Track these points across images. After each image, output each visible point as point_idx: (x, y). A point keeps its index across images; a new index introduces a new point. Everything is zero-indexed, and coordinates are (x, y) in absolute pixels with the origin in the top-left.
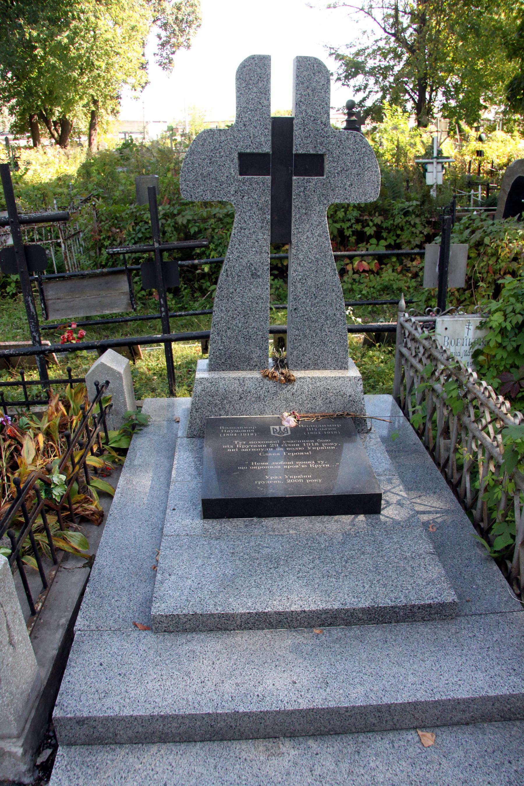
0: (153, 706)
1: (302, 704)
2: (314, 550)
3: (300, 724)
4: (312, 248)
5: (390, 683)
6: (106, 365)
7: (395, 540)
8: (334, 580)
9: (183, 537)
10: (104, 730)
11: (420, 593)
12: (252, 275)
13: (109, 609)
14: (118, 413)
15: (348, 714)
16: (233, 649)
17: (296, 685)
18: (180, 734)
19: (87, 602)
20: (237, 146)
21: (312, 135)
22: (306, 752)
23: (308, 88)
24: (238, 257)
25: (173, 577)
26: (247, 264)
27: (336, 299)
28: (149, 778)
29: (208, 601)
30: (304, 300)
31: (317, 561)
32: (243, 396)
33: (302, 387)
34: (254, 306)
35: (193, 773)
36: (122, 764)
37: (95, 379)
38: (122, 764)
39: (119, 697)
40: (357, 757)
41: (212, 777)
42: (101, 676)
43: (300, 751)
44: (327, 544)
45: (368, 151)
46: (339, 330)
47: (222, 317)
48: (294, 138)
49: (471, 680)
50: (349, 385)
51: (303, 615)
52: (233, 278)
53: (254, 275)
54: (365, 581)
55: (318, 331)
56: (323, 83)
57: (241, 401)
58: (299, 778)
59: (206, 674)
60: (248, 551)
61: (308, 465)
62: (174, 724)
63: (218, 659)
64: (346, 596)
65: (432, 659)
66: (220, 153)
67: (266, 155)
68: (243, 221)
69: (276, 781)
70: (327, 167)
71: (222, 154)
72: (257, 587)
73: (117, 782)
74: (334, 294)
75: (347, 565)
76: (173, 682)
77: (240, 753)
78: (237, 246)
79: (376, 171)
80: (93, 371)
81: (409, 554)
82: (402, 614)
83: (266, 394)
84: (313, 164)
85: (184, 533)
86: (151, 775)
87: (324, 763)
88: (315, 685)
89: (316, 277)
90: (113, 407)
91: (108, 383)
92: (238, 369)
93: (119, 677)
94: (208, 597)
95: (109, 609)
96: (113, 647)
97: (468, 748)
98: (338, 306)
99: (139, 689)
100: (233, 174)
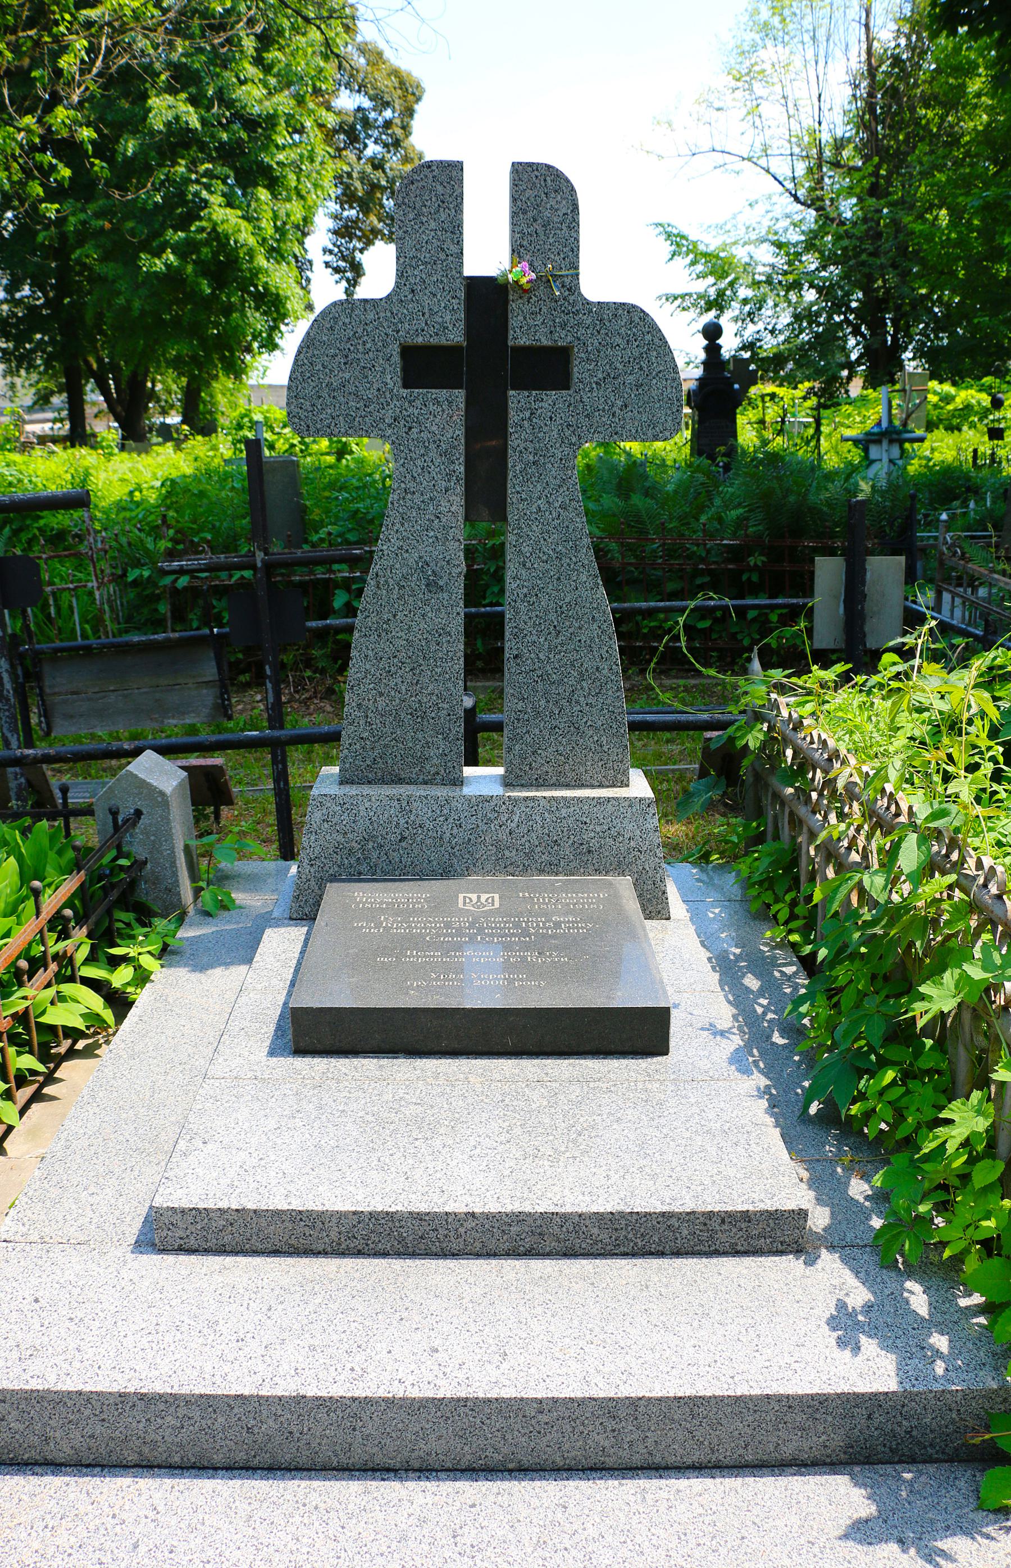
0: (127, 1377)
1: (442, 1390)
2: (514, 1111)
3: (440, 1438)
4: (548, 532)
5: (641, 1361)
6: (136, 776)
7: (693, 1100)
8: (546, 1163)
10: (22, 1427)
11: (728, 1191)
12: (427, 585)
13: (74, 1207)
14: (157, 878)
15: (544, 1418)
16: (317, 1287)
17: (436, 1355)
18: (181, 1445)
20: (398, 332)
21: (544, 309)
22: (450, 1501)
23: (535, 220)
24: (401, 548)
25: (209, 1146)
28: (102, 1531)
30: (535, 638)
31: (518, 1131)
33: (529, 817)
34: (433, 649)
36: (54, 1501)
38: (54, 1501)
39: (62, 1357)
40: (560, 1515)
41: (239, 1536)
42: (32, 1321)
43: (437, 1498)
44: (545, 1103)
46: (609, 701)
49: (822, 1362)
50: (629, 815)
51: (470, 1224)
54: (614, 1166)
55: (564, 702)
56: (564, 211)
57: (403, 844)
58: (427, 1548)
59: (250, 1327)
62: (169, 1418)
63: (281, 1303)
64: (567, 1192)
65: (742, 1321)
68: (408, 476)
69: (374, 1551)
70: (578, 370)
71: (368, 346)
72: (384, 1169)
73: (34, 1534)
74: (595, 626)
75: (580, 1139)
77: (306, 1495)
78: (398, 526)
81: (718, 1125)
83: (455, 831)
84: (550, 368)
85: (250, 1075)
86: (109, 1526)
87: (485, 1523)
89: (558, 591)
90: (149, 866)
91: (138, 813)
92: (400, 781)
93: (68, 1324)
94: (274, 1182)
95: (74, 1207)
96: (67, 1273)
97: (811, 1510)
98: (603, 652)
99: (106, 1345)
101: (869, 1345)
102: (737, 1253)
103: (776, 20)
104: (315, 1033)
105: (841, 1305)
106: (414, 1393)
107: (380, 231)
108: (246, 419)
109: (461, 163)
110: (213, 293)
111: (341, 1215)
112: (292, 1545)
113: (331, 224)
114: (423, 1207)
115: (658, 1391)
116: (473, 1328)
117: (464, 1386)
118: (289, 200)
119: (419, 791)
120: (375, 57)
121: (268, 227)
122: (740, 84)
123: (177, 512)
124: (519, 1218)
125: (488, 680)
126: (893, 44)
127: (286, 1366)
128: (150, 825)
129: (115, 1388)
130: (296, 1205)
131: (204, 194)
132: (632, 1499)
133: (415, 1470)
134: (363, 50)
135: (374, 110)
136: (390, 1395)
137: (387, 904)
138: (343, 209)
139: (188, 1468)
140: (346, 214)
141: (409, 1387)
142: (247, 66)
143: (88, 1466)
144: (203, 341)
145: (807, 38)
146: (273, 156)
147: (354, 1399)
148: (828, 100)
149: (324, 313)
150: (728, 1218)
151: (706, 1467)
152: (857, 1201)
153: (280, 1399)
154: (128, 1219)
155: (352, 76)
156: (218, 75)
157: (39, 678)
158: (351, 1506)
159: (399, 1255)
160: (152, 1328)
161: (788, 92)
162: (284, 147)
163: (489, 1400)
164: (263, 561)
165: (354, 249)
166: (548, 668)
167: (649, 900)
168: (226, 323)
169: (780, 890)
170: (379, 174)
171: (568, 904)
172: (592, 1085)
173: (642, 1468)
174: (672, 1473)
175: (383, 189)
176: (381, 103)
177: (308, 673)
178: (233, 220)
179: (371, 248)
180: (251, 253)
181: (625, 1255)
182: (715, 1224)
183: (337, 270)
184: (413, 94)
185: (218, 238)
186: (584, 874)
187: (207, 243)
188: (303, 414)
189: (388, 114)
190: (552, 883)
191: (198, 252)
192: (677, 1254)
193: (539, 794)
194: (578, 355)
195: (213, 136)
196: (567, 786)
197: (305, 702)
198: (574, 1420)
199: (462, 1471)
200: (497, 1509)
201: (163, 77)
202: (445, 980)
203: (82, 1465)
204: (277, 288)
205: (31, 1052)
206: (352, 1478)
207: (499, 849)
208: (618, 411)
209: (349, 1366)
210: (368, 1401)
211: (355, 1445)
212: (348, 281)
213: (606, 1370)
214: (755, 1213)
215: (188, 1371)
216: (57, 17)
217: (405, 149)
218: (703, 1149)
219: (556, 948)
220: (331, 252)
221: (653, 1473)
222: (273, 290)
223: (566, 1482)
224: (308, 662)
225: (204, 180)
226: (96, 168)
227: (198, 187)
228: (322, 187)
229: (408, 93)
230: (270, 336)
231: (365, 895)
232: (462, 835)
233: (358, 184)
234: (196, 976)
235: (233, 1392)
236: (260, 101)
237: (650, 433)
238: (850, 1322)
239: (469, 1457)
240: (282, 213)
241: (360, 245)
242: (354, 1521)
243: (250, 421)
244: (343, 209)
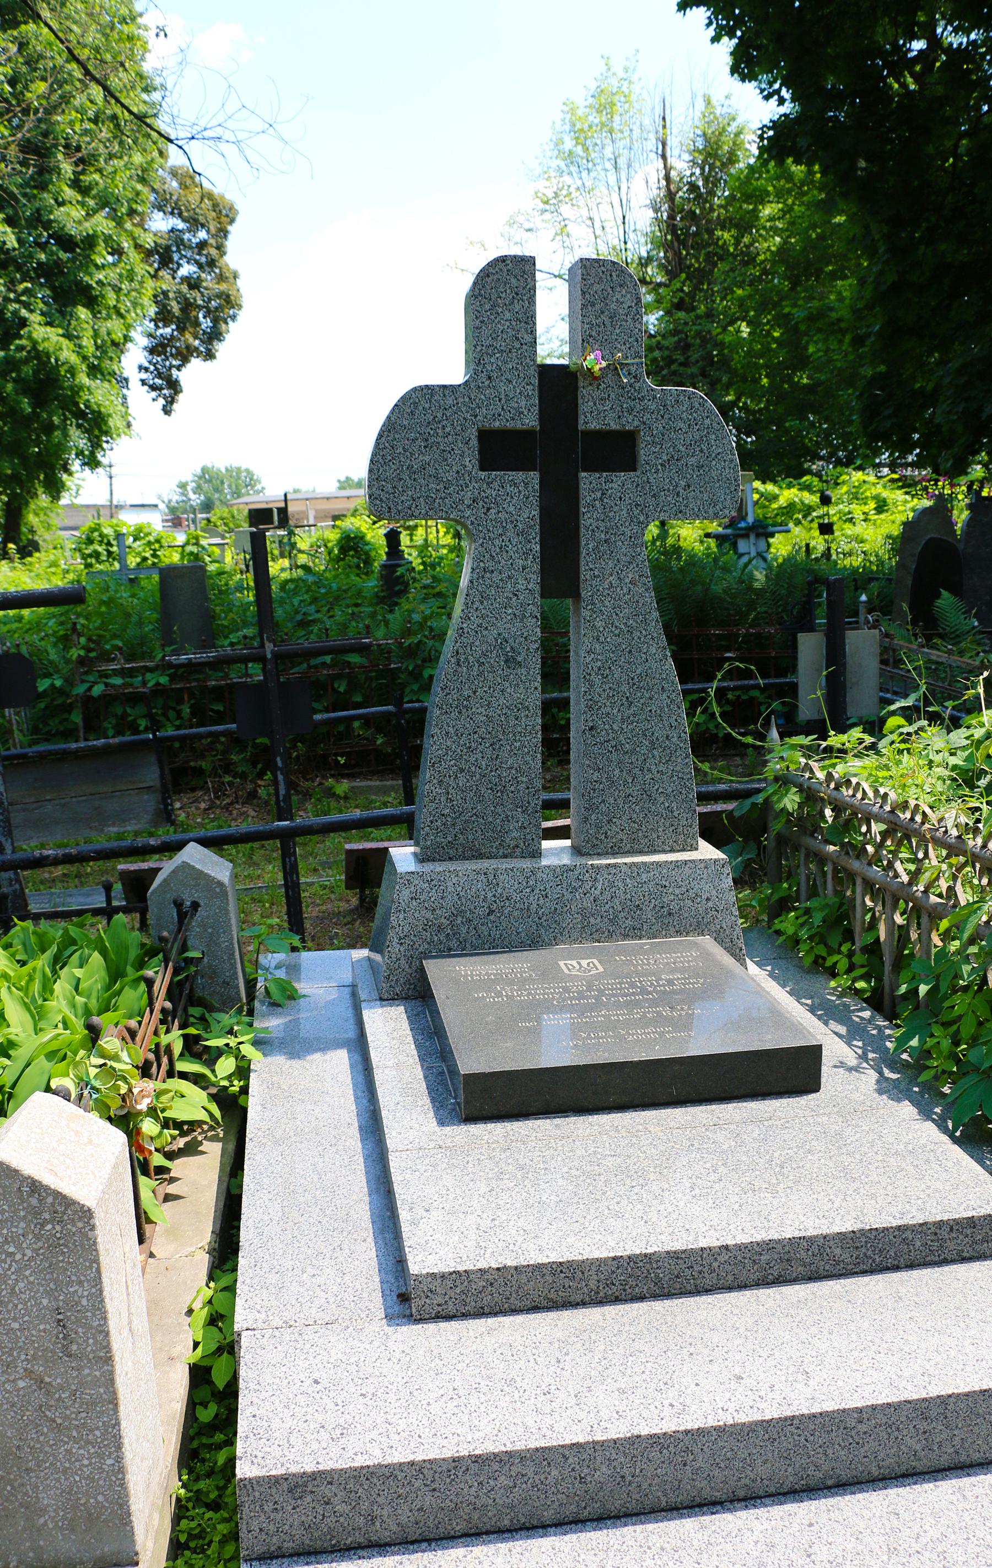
0: (454, 1442)
1: (767, 1411)
5: (932, 1363)
6: (193, 867)
9: (432, 1152)
12: (506, 661)
14: (214, 972)
15: (862, 1428)
19: (248, 1281)
20: (476, 416)
21: (612, 395)
22: (787, 1524)
23: (603, 312)
24: (480, 626)
25: (434, 1213)
26: (496, 640)
27: (668, 706)
29: (525, 1246)
30: (609, 709)
31: (723, 1170)
32: (494, 907)
33: (612, 884)
34: (512, 723)
37: (170, 896)
40: (896, 1522)
42: (323, 1402)
43: (773, 1523)
46: (678, 768)
48: (580, 401)
50: (705, 876)
52: (469, 668)
53: (511, 662)
57: (492, 917)
59: (548, 1380)
60: (576, 1163)
61: (657, 1012)
64: (802, 1218)
67: (526, 435)
68: (487, 556)
70: (644, 453)
71: (448, 430)
72: (618, 1216)
74: (664, 696)
75: (785, 1171)
76: (483, 1398)
78: (477, 604)
79: (731, 461)
80: (165, 880)
83: (541, 902)
85: (432, 1145)
88: (783, 1378)
89: (629, 663)
92: (481, 856)
94: (520, 1239)
95: (301, 1290)
96: (333, 1352)
100: (469, 468)
102: (963, 1260)
103: (579, 150)
106: (742, 1418)
107: (196, 349)
108: (96, 534)
109: (534, 258)
110: (34, 411)
111: (600, 1262)
113: (145, 342)
114: (677, 1246)
115: (963, 1389)
117: (786, 1407)
118: (109, 317)
119: (504, 864)
120: (188, 178)
121: (88, 343)
122: (547, 207)
123: (87, 619)
124: (769, 1246)
126: (688, 173)
128: (208, 917)
129: (447, 1454)
130: (554, 1257)
131: (24, 313)
132: (954, 1498)
133: (739, 1500)
134: (174, 173)
136: (721, 1423)
139: (516, 1530)
140: (160, 331)
141: (735, 1414)
142: (66, 189)
143: (412, 1543)
144: (24, 459)
145: (609, 166)
146: (91, 275)
147: (687, 1432)
148: (632, 223)
150: (956, 1226)
153: (615, 1441)
154: (365, 1295)
156: (35, 197)
158: (695, 1543)
159: (655, 1297)
160: (451, 1392)
161: (594, 214)
162: (103, 266)
164: (272, 652)
165: (171, 366)
166: (622, 738)
168: (48, 441)
169: (834, 941)
170: (195, 293)
171: (668, 964)
173: (950, 1469)
174: (977, 1470)
175: (200, 308)
176: (195, 223)
177: (227, 779)
178: (55, 339)
179: (188, 365)
180: (72, 371)
181: (864, 1272)
183: (153, 388)
184: (227, 216)
185: (38, 356)
187: (26, 361)
188: (384, 496)
189: (202, 235)
191: (18, 371)
192: (911, 1266)
193: (619, 861)
194: (644, 439)
196: (641, 852)
197: (227, 808)
198: (890, 1426)
199: (784, 1494)
202: (599, 1038)
203: (407, 1543)
204: (99, 405)
206: (682, 1516)
207: (585, 917)
209: (666, 1403)
210: (701, 1432)
212: (165, 398)
213: (906, 1374)
214: (979, 1218)
215: (512, 1428)
220: (146, 370)
221: (959, 1472)
222: (95, 407)
223: (885, 1492)
224: (227, 767)
225: (24, 298)
227: (17, 306)
229: (222, 216)
230: (92, 453)
232: (549, 905)
233: (174, 304)
234: (296, 1063)
235: (568, 1442)
236: (80, 222)
237: (711, 511)
239: (791, 1479)
240: (103, 331)
242: (706, 1556)
243: (100, 535)
244: (157, 327)
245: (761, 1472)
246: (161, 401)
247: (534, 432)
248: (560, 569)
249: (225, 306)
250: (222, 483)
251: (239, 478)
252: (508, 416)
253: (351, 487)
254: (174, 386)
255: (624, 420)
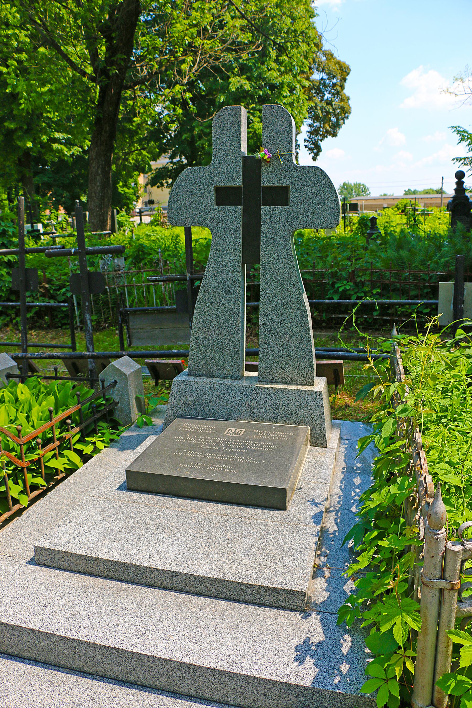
5: (201, 647)
21: (277, 170)
23: (273, 131)
24: (214, 275)
27: (301, 317)
30: (272, 316)
33: (265, 396)
35: (5, 682)
41: (18, 689)
44: (218, 525)
45: (327, 183)
46: (305, 346)
47: (200, 328)
50: (310, 398)
52: (209, 293)
57: (211, 404)
66: (199, 186)
67: (238, 188)
68: (218, 244)
71: (201, 187)
82: (249, 593)
83: (233, 400)
84: (279, 196)
89: (282, 295)
92: (213, 376)
98: (302, 324)
101: (309, 662)
104: (136, 482)
105: (308, 640)
112: (35, 698)
113: (308, 129)
116: (138, 619)
120: (329, 56)
125: (327, 332)
127: (55, 621)
134: (325, 54)
135: (328, 79)
137: (195, 429)
138: (314, 123)
142: (272, 63)
146: (282, 101)
149: (316, 169)
151: (222, 703)
152: (345, 592)
155: (319, 65)
156: (259, 67)
157: (127, 322)
162: (286, 97)
163: (127, 651)
164: (189, 277)
165: (318, 139)
167: (318, 438)
170: (329, 107)
171: (272, 437)
172: (243, 520)
176: (331, 76)
182: (262, 592)
183: (310, 149)
184: (346, 72)
186: (288, 424)
189: (334, 81)
190: (272, 426)
193: (270, 386)
194: (292, 189)
195: (256, 93)
196: (286, 383)
200: (124, 701)
201: (236, 70)
205: (42, 477)
208: (310, 215)
209: (80, 625)
211: (76, 660)
216: (177, 50)
217: (341, 96)
218: (275, 556)
219: (254, 456)
220: (308, 141)
221: (199, 700)
225: (252, 111)
226: (191, 109)
228: (302, 113)
229: (344, 71)
231: (188, 425)
232: (236, 402)
233: (320, 112)
234: (121, 453)
236: (277, 78)
237: (324, 225)
238: (306, 649)
239: (121, 675)
241: (320, 138)
245: (108, 667)
246: (313, 154)
247: (241, 187)
248: (251, 251)
249: (344, 112)
250: (352, 190)
251: (360, 188)
252: (228, 180)
253: (410, 194)
254: (319, 149)
255: (282, 182)
